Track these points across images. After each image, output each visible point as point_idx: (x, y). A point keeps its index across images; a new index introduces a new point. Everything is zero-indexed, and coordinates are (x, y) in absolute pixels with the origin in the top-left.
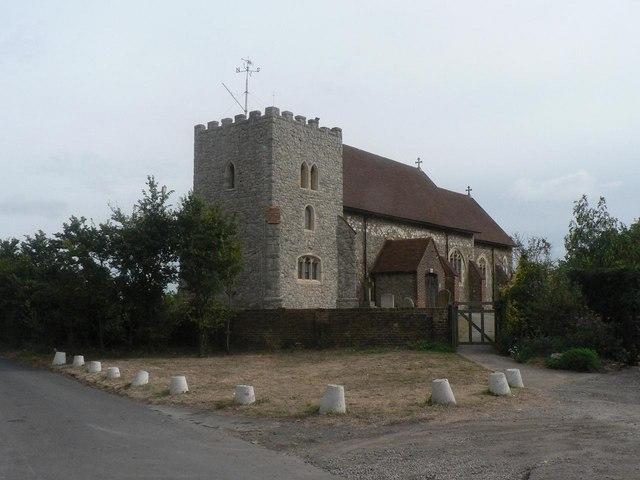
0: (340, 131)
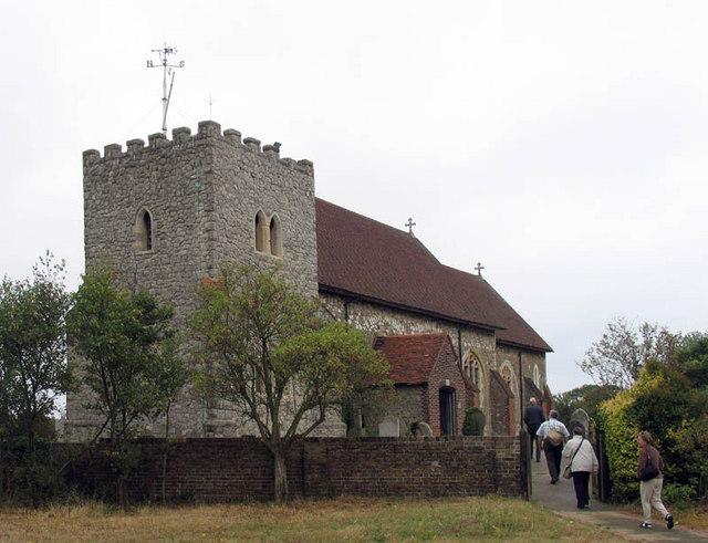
0: (311, 165)
